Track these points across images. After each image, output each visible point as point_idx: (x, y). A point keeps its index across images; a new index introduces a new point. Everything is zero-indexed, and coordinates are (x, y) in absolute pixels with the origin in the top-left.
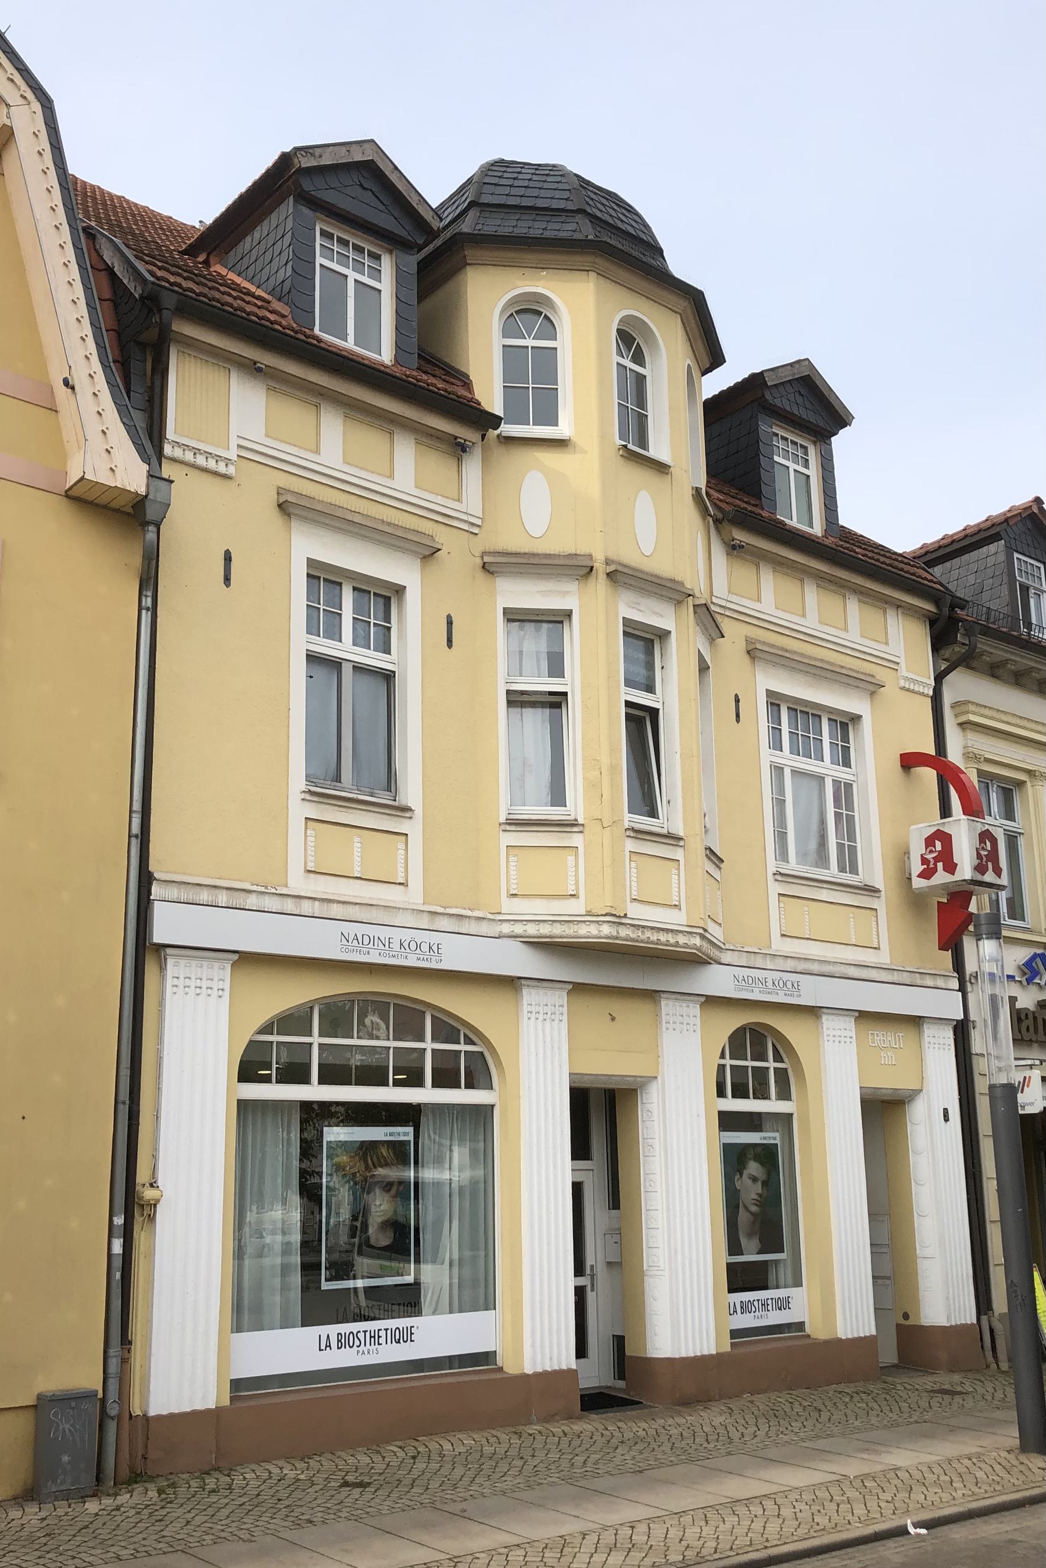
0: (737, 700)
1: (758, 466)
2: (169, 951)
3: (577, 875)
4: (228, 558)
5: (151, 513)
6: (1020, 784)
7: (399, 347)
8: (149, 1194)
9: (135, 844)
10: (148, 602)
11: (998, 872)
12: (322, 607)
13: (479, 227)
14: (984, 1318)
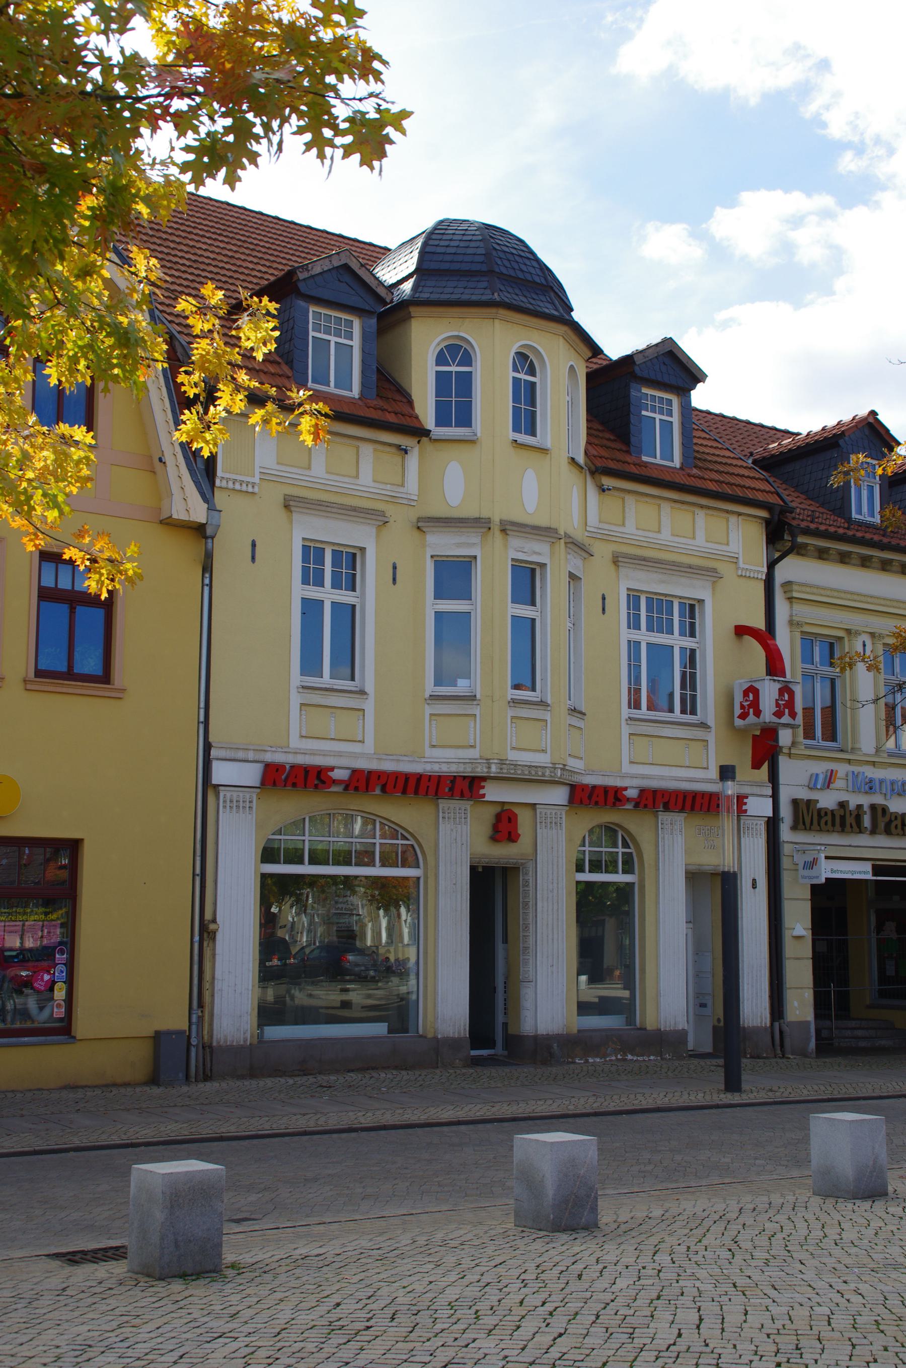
0: (604, 598)
1: (628, 423)
2: (221, 788)
3: (475, 734)
4: (254, 545)
5: (209, 531)
6: (840, 639)
7: (364, 385)
8: (212, 927)
9: (202, 727)
10: (207, 581)
11: (793, 715)
12: (312, 566)
13: (417, 295)
14: (777, 1025)
